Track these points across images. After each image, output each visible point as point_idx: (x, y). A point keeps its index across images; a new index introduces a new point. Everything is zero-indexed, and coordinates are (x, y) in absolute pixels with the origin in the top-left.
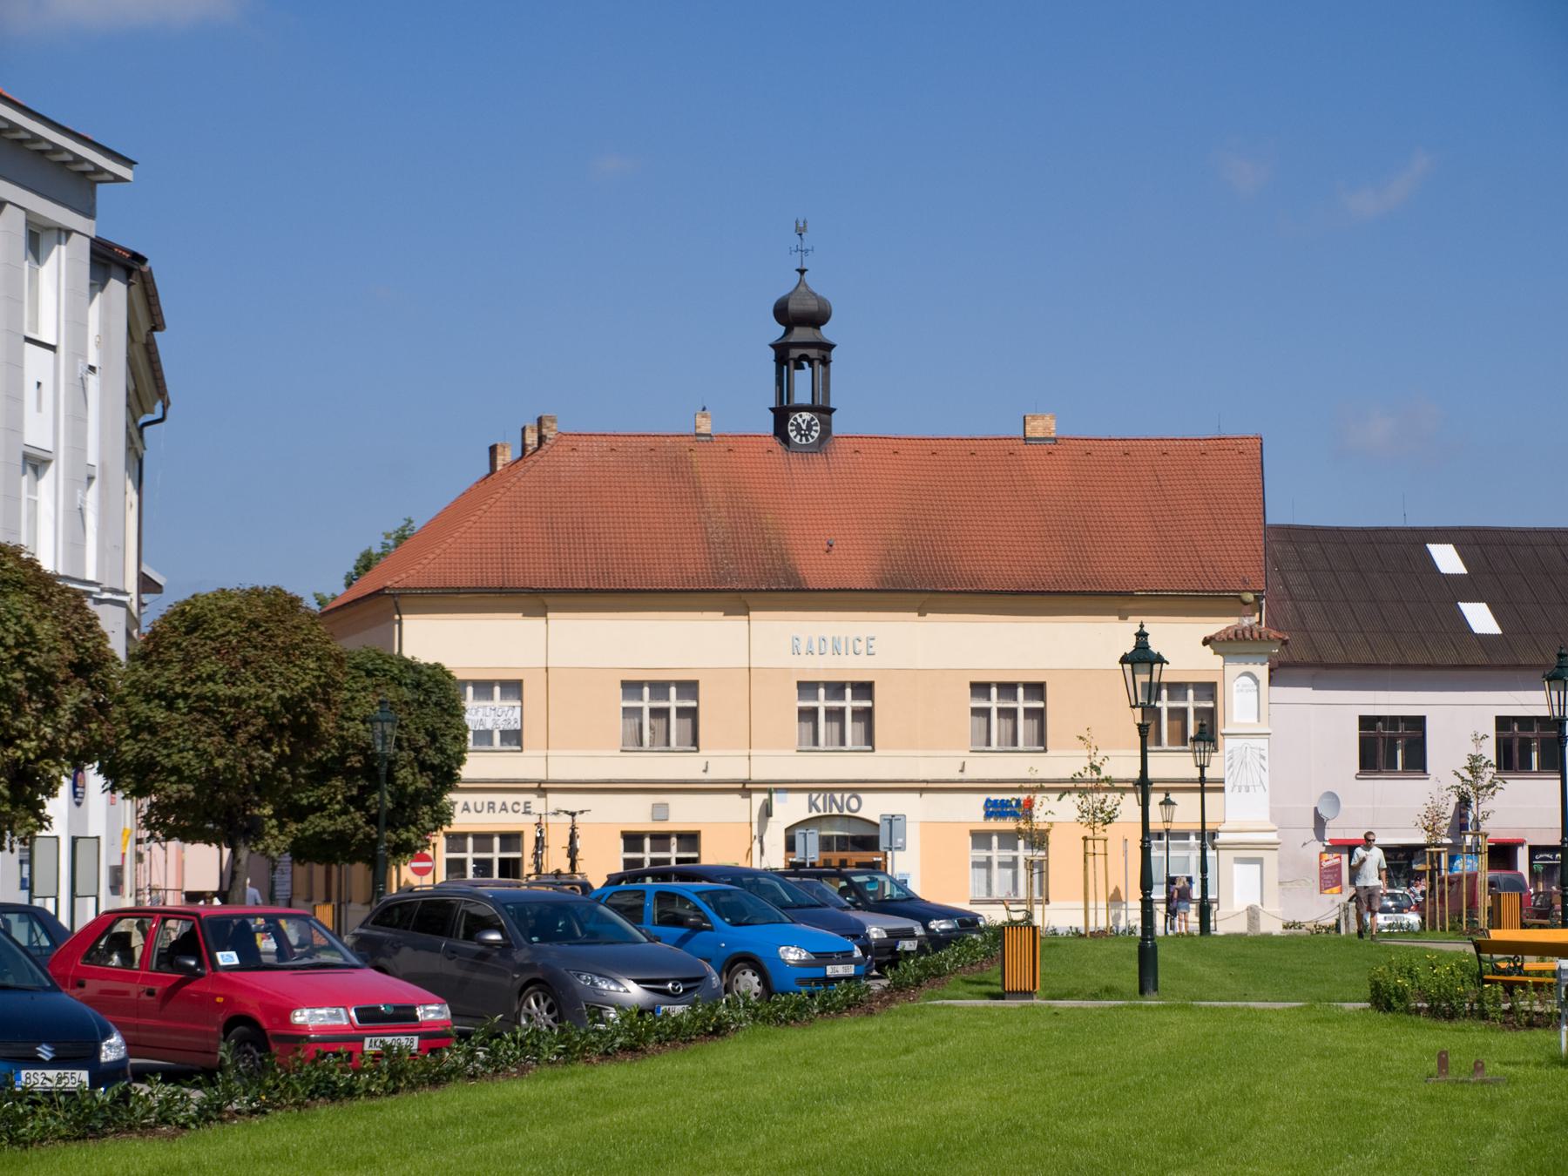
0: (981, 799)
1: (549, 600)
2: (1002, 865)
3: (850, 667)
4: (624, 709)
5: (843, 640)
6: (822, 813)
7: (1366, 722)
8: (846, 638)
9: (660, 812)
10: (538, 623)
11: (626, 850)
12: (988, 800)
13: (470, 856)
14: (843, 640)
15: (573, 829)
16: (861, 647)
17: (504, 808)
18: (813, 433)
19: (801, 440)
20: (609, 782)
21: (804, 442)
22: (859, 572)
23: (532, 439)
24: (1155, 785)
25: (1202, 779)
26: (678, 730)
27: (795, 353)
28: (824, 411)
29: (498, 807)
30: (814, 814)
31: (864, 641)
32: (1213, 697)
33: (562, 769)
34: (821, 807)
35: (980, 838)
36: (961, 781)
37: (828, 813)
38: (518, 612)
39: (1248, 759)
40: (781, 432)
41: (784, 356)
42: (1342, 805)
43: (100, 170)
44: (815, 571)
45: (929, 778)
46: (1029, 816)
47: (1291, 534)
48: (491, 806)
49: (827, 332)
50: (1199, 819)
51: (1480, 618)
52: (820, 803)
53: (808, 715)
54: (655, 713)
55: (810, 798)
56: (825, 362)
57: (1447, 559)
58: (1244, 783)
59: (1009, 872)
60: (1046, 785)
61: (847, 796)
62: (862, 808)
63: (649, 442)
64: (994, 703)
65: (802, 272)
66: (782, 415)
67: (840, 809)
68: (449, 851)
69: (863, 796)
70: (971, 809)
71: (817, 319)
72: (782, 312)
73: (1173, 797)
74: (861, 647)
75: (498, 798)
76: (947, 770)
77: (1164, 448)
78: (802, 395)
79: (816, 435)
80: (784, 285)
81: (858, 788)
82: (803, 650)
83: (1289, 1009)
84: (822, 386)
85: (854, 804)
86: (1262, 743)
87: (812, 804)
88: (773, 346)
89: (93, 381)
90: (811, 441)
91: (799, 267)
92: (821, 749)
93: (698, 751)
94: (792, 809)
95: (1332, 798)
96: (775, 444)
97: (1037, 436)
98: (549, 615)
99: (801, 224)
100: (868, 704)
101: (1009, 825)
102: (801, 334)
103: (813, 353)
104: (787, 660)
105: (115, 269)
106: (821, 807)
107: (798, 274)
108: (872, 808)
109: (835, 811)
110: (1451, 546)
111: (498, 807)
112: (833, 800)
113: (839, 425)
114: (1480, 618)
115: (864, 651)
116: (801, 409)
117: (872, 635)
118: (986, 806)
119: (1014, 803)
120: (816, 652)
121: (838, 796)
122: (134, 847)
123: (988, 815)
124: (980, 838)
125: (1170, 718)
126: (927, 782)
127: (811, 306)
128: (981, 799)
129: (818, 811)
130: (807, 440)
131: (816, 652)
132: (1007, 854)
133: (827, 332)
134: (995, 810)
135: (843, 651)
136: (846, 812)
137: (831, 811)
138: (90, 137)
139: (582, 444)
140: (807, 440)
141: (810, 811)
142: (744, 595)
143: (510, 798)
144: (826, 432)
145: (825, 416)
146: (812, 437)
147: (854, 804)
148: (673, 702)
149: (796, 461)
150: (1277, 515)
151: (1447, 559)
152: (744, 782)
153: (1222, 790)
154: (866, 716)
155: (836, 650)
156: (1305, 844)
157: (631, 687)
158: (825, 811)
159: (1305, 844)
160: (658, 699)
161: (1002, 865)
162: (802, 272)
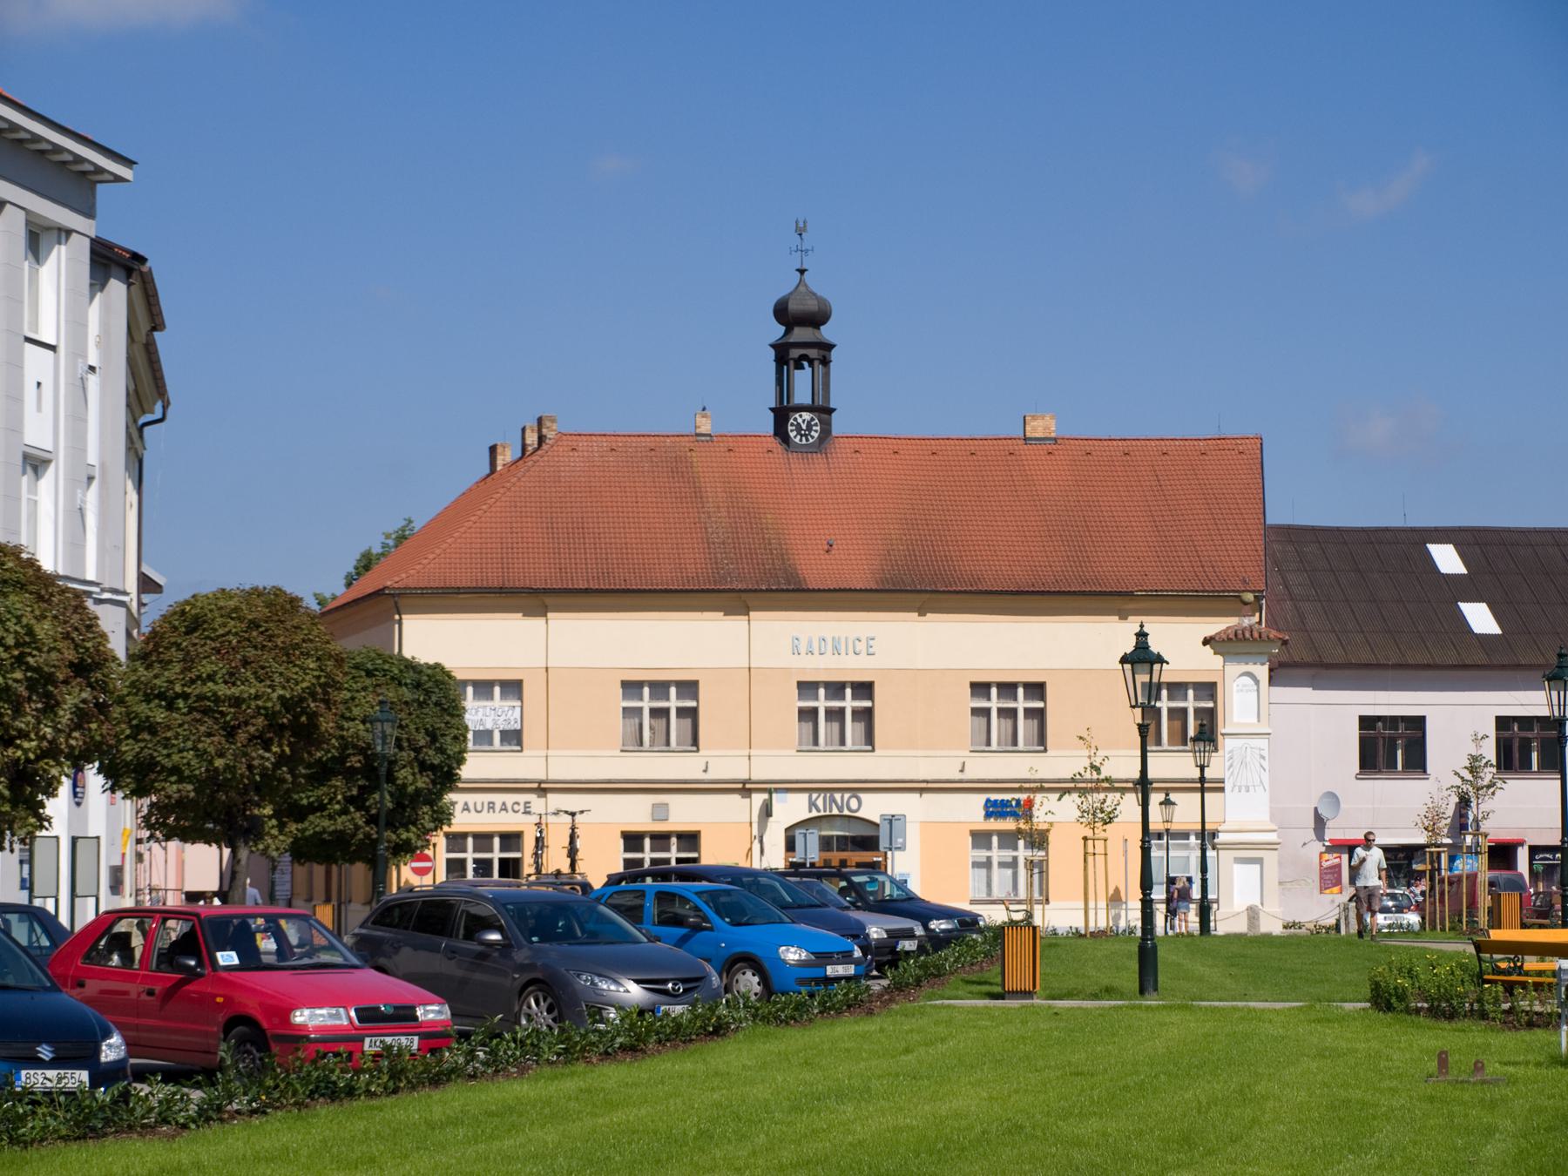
0: (981, 799)
1: (549, 600)
2: (1002, 865)
3: (850, 667)
4: (624, 709)
5: (843, 640)
6: (822, 813)
7: (1366, 722)
8: (846, 638)
9: (660, 812)
10: (538, 623)
11: (626, 850)
12: (988, 800)
13: (470, 856)
14: (843, 640)
15: (573, 829)
16: (861, 647)
17: (504, 808)
18: (813, 433)
19: (801, 440)
20: (609, 782)
21: (804, 442)
22: (859, 572)
23: (532, 439)
24: (1155, 785)
25: (1202, 779)
26: (678, 730)
27: (795, 353)
28: (824, 411)
29: (498, 807)
30: (814, 814)
31: (864, 641)
32: (1213, 697)
33: (562, 769)
34: (821, 807)
35: (980, 838)
36: (961, 781)
37: (828, 813)
38: (518, 612)
39: (1248, 759)
40: (781, 432)
41: (784, 356)
42: (1342, 805)
43: (100, 170)
44: (815, 571)
45: (929, 778)
46: (1029, 816)
47: (1291, 534)
48: (491, 806)
49: (827, 332)
50: (1199, 819)
51: (1480, 618)
52: (820, 803)
53: (808, 715)
54: (655, 713)
55: (810, 798)
56: (825, 362)
57: (1447, 559)
58: (1244, 783)
59: (1009, 872)
60: (1046, 785)
61: (847, 796)
62: (862, 808)
63: (649, 442)
64: (994, 703)
65: (802, 272)
66: (782, 415)
67: (840, 809)
68: (449, 851)
69: (863, 796)
70: (971, 809)
71: (817, 319)
72: (782, 312)
73: (1173, 797)
74: (861, 647)
75: (498, 798)
76: (947, 770)
77: (1164, 448)
78: (802, 395)
79: (816, 435)
80: (784, 285)
81: (858, 788)
82: (803, 650)
83: (1289, 1009)
84: (822, 386)
85: (854, 804)
86: (1262, 743)
87: (812, 804)
88: (773, 346)
89: (93, 381)
90: (811, 441)
91: (799, 267)
92: (821, 749)
93: (698, 751)
94: (792, 809)
95: (1332, 798)
96: (775, 444)
97: (1037, 436)
98: (549, 615)
99: (801, 224)
100: (868, 704)
101: (1009, 825)
102: (801, 334)
103: (813, 353)
104: (787, 660)
105: (115, 269)
106: (821, 807)
107: (798, 274)
108: (872, 808)
109: (835, 811)
110: (1451, 546)
111: (498, 807)
112: (833, 800)
113: (839, 425)
114: (1480, 618)
115: (864, 651)
116: (801, 409)
117: (872, 635)
118: (986, 806)
119: (1014, 803)
120: (816, 652)
121: (838, 796)
122: (134, 847)
123: (988, 815)
124: (980, 838)
125: (1170, 718)
126: (927, 782)
127: (811, 306)
128: (981, 799)
129: (818, 811)
130: (807, 440)
131: (816, 652)
132: (1007, 854)
133: (827, 332)
134: (995, 810)
135: (843, 651)
136: (846, 812)
137: (831, 811)
138: (90, 137)
139: (582, 444)
140: (807, 440)
141: (810, 811)
142: (744, 595)
143: (510, 798)
144: (826, 432)
145: (825, 416)
146: (812, 437)
147: (854, 804)
148: (673, 702)
149: (796, 461)
150: (1277, 515)
151: (1447, 559)
152: (744, 782)
153: (1222, 790)
154: (866, 716)
155: (836, 650)
156: (1305, 844)
157: (631, 687)
158: (825, 811)
159: (1305, 844)
160: (658, 699)
161: (1002, 865)
162: (802, 272)
